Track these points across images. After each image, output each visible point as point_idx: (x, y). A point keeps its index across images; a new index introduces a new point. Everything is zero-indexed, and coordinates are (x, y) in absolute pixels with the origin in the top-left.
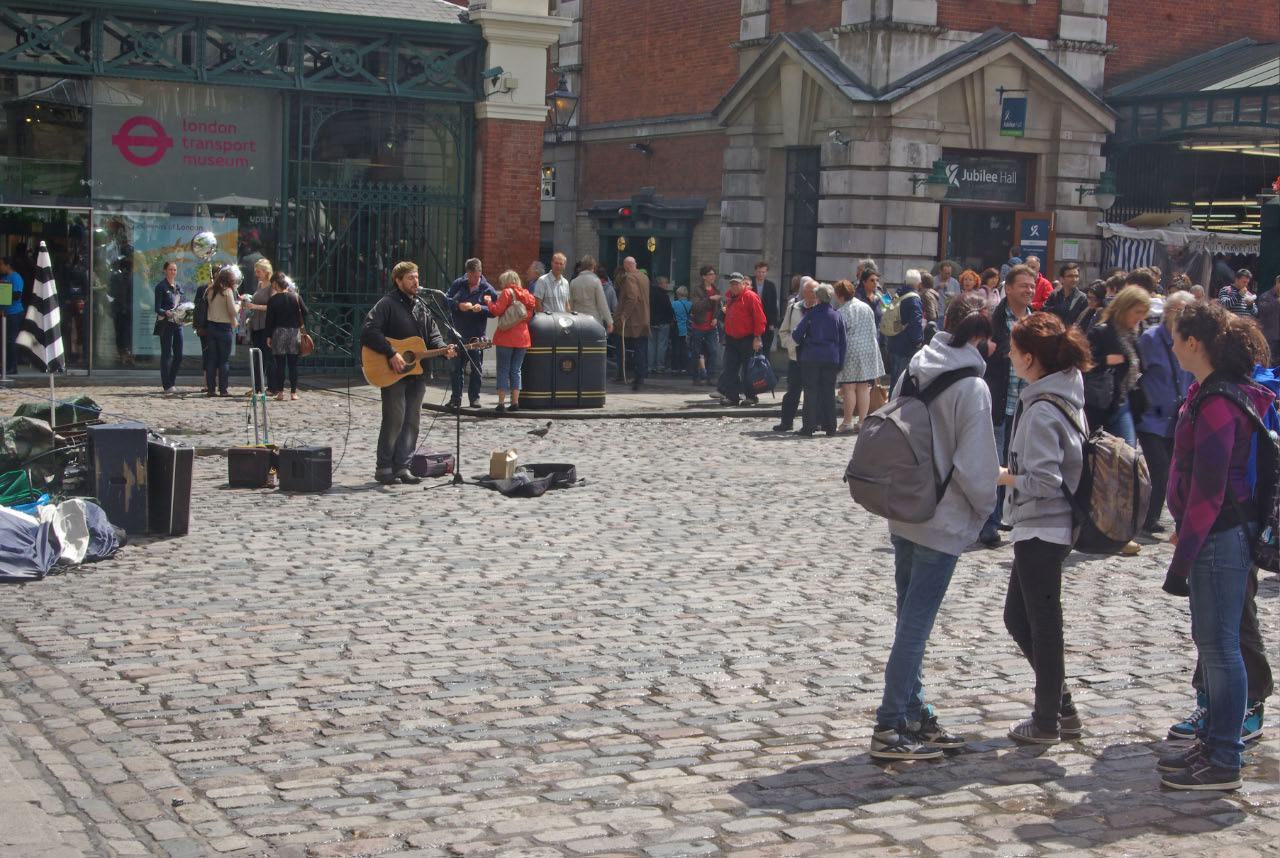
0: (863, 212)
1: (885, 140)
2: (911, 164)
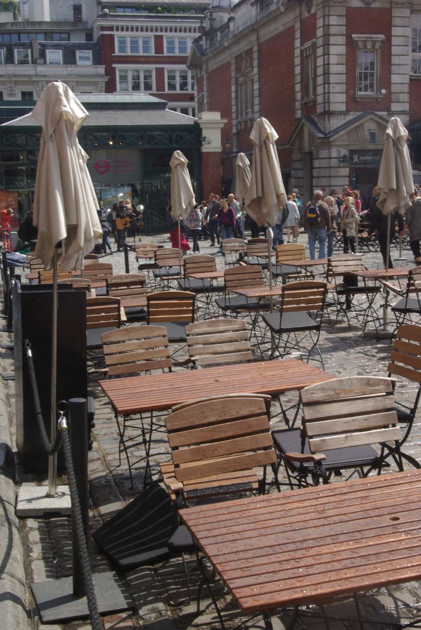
0: (324, 172)
1: (329, 149)
2: (338, 156)
